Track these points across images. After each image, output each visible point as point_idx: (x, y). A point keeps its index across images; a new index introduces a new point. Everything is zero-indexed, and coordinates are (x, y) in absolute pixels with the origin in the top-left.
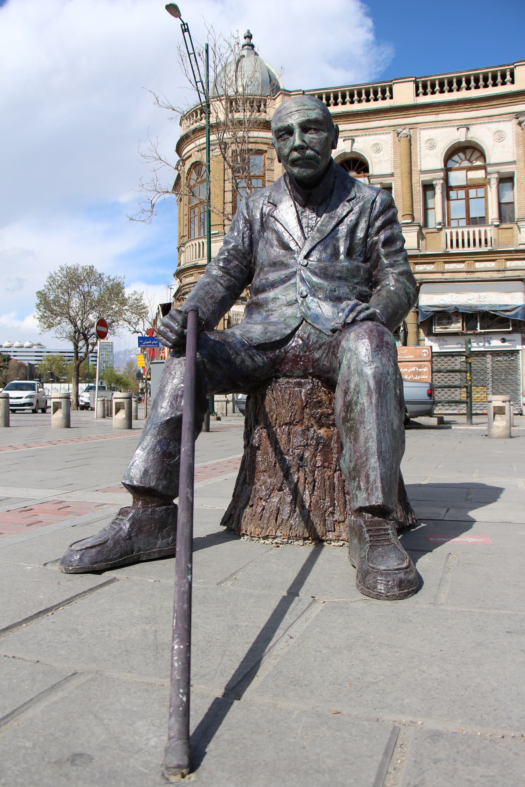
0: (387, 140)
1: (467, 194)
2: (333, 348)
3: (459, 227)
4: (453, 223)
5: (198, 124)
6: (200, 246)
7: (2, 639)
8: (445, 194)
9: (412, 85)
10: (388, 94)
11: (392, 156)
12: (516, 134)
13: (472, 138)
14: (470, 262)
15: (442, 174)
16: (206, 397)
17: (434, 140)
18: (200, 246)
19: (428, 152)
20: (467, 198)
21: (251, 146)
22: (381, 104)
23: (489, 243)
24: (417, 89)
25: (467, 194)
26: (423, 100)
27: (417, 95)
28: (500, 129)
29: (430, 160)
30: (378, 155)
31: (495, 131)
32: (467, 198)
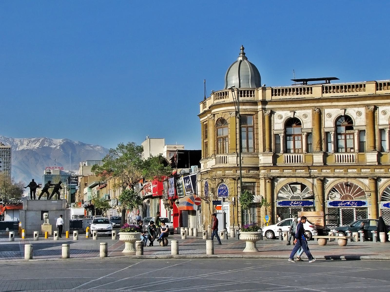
0: (309, 112)
1: (346, 137)
2: (339, 148)
3: (342, 152)
4: (340, 150)
5: (218, 100)
6: (221, 158)
7: (1, 239)
8: (336, 137)
9: (320, 88)
10: (310, 91)
11: (312, 120)
12: (366, 113)
13: (347, 114)
14: (345, 169)
15: (334, 129)
16: (293, 123)
17: (331, 114)
18: (221, 158)
19: (328, 119)
20: (346, 139)
21: (217, 177)
22: (307, 96)
23: (354, 161)
24: (323, 89)
25: (346, 137)
26: (325, 95)
27: (323, 93)
28: (359, 110)
29: (329, 124)
30: (305, 119)
31: (357, 111)
32: (346, 139)
